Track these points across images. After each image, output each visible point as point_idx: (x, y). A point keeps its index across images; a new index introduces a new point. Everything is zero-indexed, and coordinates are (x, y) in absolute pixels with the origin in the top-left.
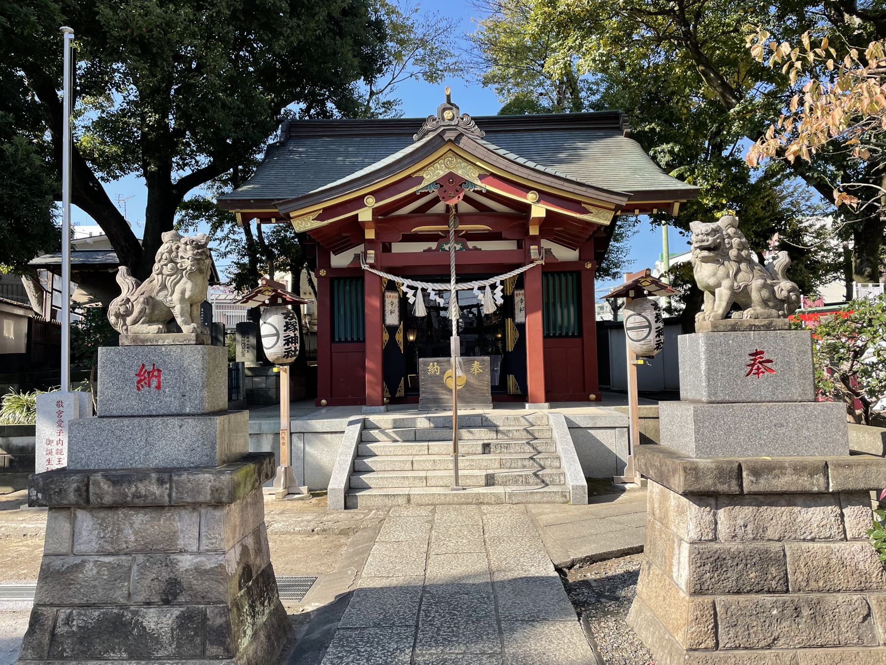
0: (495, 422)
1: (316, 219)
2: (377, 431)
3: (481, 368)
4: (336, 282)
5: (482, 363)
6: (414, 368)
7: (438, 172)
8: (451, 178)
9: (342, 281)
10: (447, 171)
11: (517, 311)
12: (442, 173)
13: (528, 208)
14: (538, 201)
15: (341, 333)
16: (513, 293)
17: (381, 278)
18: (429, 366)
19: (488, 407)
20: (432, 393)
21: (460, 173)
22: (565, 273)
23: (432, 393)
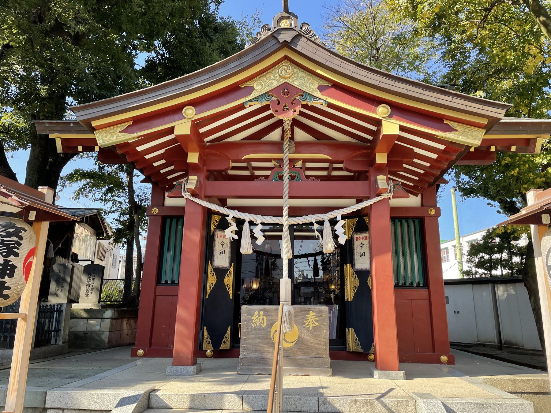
1: (124, 131)
3: (319, 319)
4: (168, 221)
6: (236, 319)
7: (272, 81)
8: (286, 90)
9: (175, 221)
10: (282, 81)
11: (357, 257)
12: (275, 84)
13: (378, 123)
14: (390, 116)
15: (167, 276)
18: (253, 316)
19: (325, 373)
20: (256, 351)
21: (296, 83)
22: (407, 219)
23: (256, 351)
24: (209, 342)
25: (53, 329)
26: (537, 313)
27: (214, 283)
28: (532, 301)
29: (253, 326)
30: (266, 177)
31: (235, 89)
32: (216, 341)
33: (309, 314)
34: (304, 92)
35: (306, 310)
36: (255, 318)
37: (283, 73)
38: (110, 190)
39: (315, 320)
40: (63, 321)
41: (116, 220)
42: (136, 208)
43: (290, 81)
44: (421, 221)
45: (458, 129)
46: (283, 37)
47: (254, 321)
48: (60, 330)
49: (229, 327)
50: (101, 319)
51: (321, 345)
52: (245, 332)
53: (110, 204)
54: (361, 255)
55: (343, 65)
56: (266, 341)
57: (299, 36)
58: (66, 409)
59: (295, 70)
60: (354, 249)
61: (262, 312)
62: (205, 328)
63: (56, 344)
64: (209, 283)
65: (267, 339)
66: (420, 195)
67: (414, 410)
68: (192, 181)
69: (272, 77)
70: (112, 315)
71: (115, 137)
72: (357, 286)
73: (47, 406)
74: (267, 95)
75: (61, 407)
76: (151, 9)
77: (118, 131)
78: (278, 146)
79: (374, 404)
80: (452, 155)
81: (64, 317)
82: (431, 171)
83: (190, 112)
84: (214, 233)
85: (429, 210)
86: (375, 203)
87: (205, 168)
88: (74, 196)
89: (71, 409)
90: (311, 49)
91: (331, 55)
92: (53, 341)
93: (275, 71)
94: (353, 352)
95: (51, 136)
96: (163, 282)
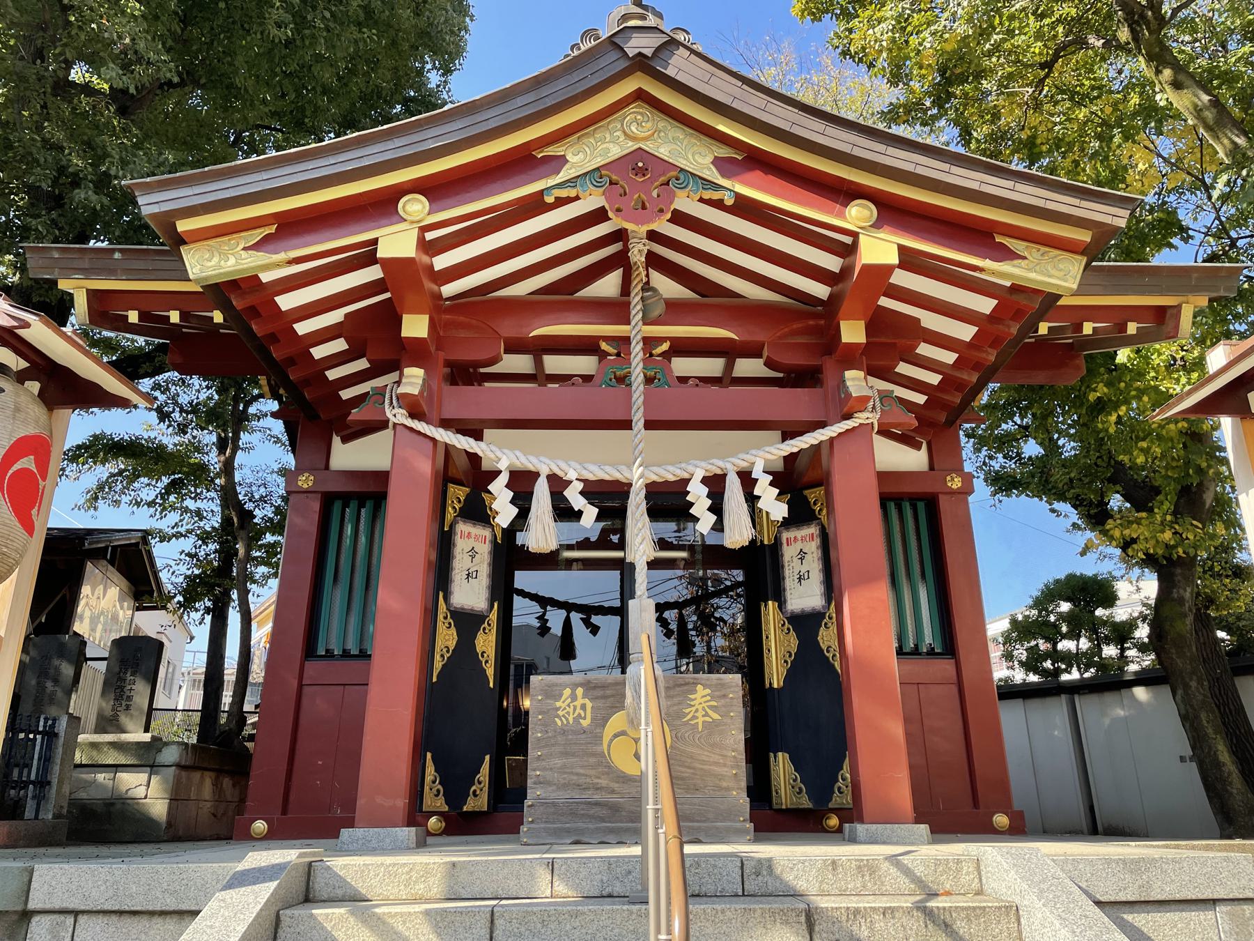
0: (789, 877)
1: (256, 247)
2: (339, 911)
4: (337, 506)
5: (719, 692)
7: (607, 147)
10: (631, 146)
11: (790, 583)
12: (615, 152)
13: (848, 250)
14: (877, 225)
15: (332, 637)
16: (778, 540)
17: (433, 440)
21: (663, 152)
24: (438, 791)
25: (33, 777)
26: (1192, 725)
27: (452, 646)
28: (1178, 697)
29: (559, 723)
30: (587, 378)
31: (521, 162)
32: (456, 788)
33: (695, 692)
34: (682, 170)
35: (687, 684)
36: (563, 706)
37: (633, 129)
38: (174, 487)
39: (711, 707)
40: (58, 761)
41: (189, 555)
42: (237, 523)
43: (648, 146)
44: (931, 503)
45: (1026, 254)
46: (639, 44)
47: (560, 713)
48: (49, 783)
49: (487, 758)
50: (152, 766)
51: (725, 765)
52: (539, 739)
53: (173, 517)
54: (800, 579)
55: (770, 107)
56: (592, 760)
57: (672, 44)
58: (83, 912)
59: (661, 125)
60: (783, 566)
61: (580, 691)
62: (429, 755)
63: (36, 817)
64: (439, 644)
65: (594, 755)
66: (924, 446)
67: (976, 880)
68: (413, 380)
69: (608, 136)
70: (181, 756)
71: (232, 261)
72: (794, 650)
73: (32, 905)
74: (596, 175)
75: (71, 906)
76: (307, 43)
77: (241, 246)
78: (616, 309)
79: (880, 869)
80: (1009, 327)
81: (60, 750)
82: (958, 374)
83: (415, 207)
84: (452, 526)
85: (949, 478)
86: (840, 434)
87: (442, 356)
88: (83, 501)
89: (98, 912)
90: (698, 73)
91: (745, 87)
92: (29, 814)
93: (614, 123)
94: (788, 810)
95: (63, 285)
96: (321, 651)
